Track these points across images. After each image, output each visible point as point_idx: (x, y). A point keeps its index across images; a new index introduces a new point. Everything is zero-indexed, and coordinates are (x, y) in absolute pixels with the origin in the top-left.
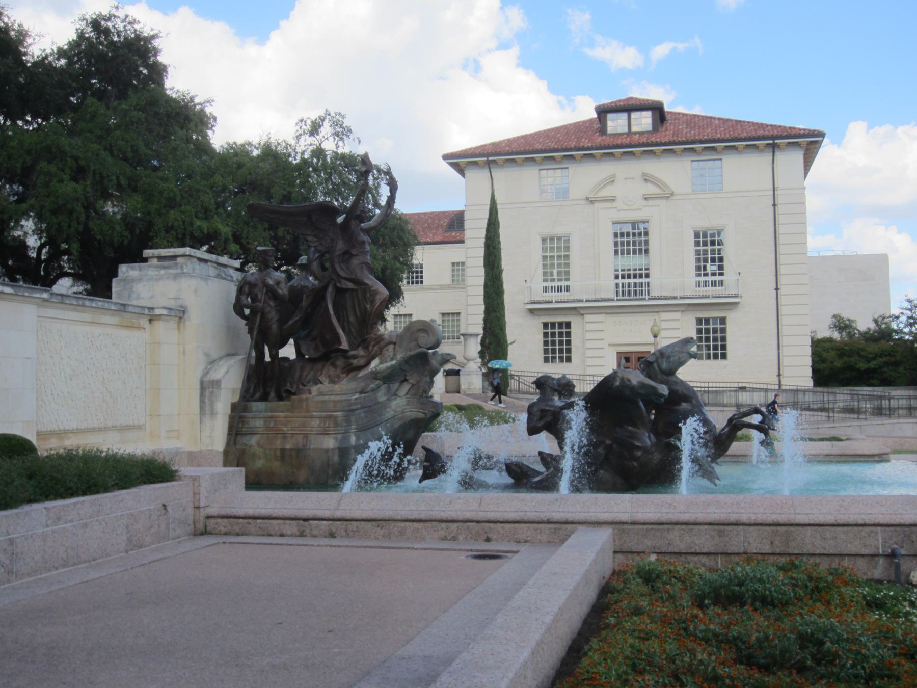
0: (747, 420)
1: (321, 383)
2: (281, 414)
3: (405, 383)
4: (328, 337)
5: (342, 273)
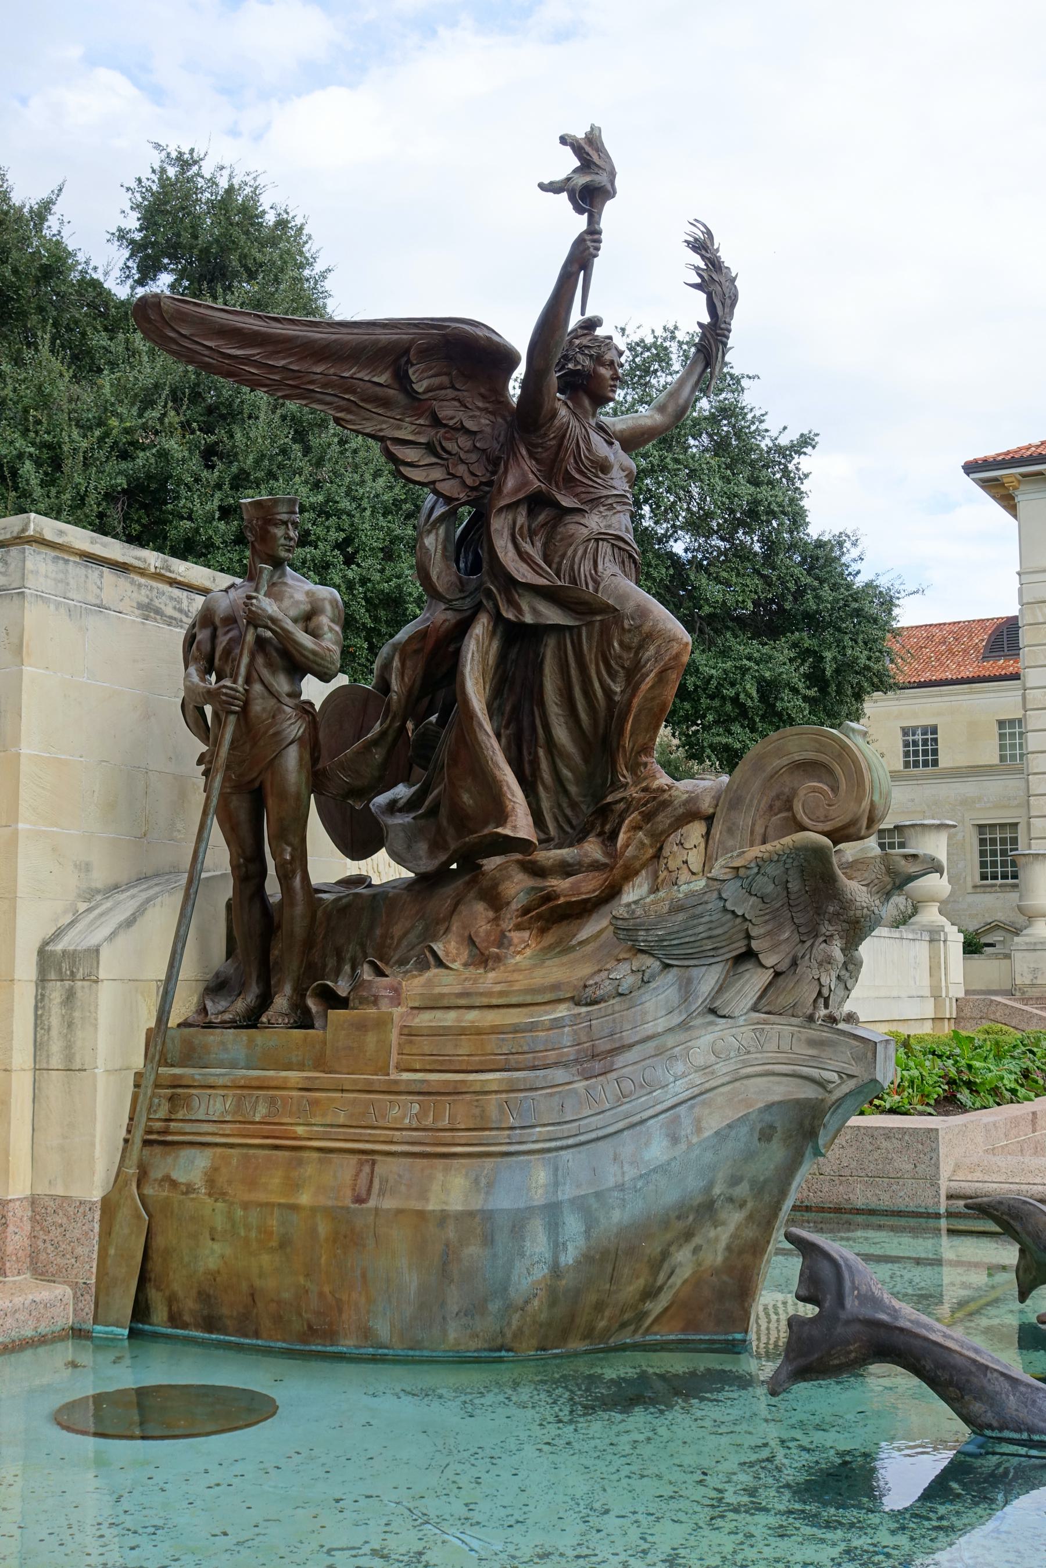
1: (440, 963)
2: (294, 1076)
3: (749, 965)
4: (466, 799)
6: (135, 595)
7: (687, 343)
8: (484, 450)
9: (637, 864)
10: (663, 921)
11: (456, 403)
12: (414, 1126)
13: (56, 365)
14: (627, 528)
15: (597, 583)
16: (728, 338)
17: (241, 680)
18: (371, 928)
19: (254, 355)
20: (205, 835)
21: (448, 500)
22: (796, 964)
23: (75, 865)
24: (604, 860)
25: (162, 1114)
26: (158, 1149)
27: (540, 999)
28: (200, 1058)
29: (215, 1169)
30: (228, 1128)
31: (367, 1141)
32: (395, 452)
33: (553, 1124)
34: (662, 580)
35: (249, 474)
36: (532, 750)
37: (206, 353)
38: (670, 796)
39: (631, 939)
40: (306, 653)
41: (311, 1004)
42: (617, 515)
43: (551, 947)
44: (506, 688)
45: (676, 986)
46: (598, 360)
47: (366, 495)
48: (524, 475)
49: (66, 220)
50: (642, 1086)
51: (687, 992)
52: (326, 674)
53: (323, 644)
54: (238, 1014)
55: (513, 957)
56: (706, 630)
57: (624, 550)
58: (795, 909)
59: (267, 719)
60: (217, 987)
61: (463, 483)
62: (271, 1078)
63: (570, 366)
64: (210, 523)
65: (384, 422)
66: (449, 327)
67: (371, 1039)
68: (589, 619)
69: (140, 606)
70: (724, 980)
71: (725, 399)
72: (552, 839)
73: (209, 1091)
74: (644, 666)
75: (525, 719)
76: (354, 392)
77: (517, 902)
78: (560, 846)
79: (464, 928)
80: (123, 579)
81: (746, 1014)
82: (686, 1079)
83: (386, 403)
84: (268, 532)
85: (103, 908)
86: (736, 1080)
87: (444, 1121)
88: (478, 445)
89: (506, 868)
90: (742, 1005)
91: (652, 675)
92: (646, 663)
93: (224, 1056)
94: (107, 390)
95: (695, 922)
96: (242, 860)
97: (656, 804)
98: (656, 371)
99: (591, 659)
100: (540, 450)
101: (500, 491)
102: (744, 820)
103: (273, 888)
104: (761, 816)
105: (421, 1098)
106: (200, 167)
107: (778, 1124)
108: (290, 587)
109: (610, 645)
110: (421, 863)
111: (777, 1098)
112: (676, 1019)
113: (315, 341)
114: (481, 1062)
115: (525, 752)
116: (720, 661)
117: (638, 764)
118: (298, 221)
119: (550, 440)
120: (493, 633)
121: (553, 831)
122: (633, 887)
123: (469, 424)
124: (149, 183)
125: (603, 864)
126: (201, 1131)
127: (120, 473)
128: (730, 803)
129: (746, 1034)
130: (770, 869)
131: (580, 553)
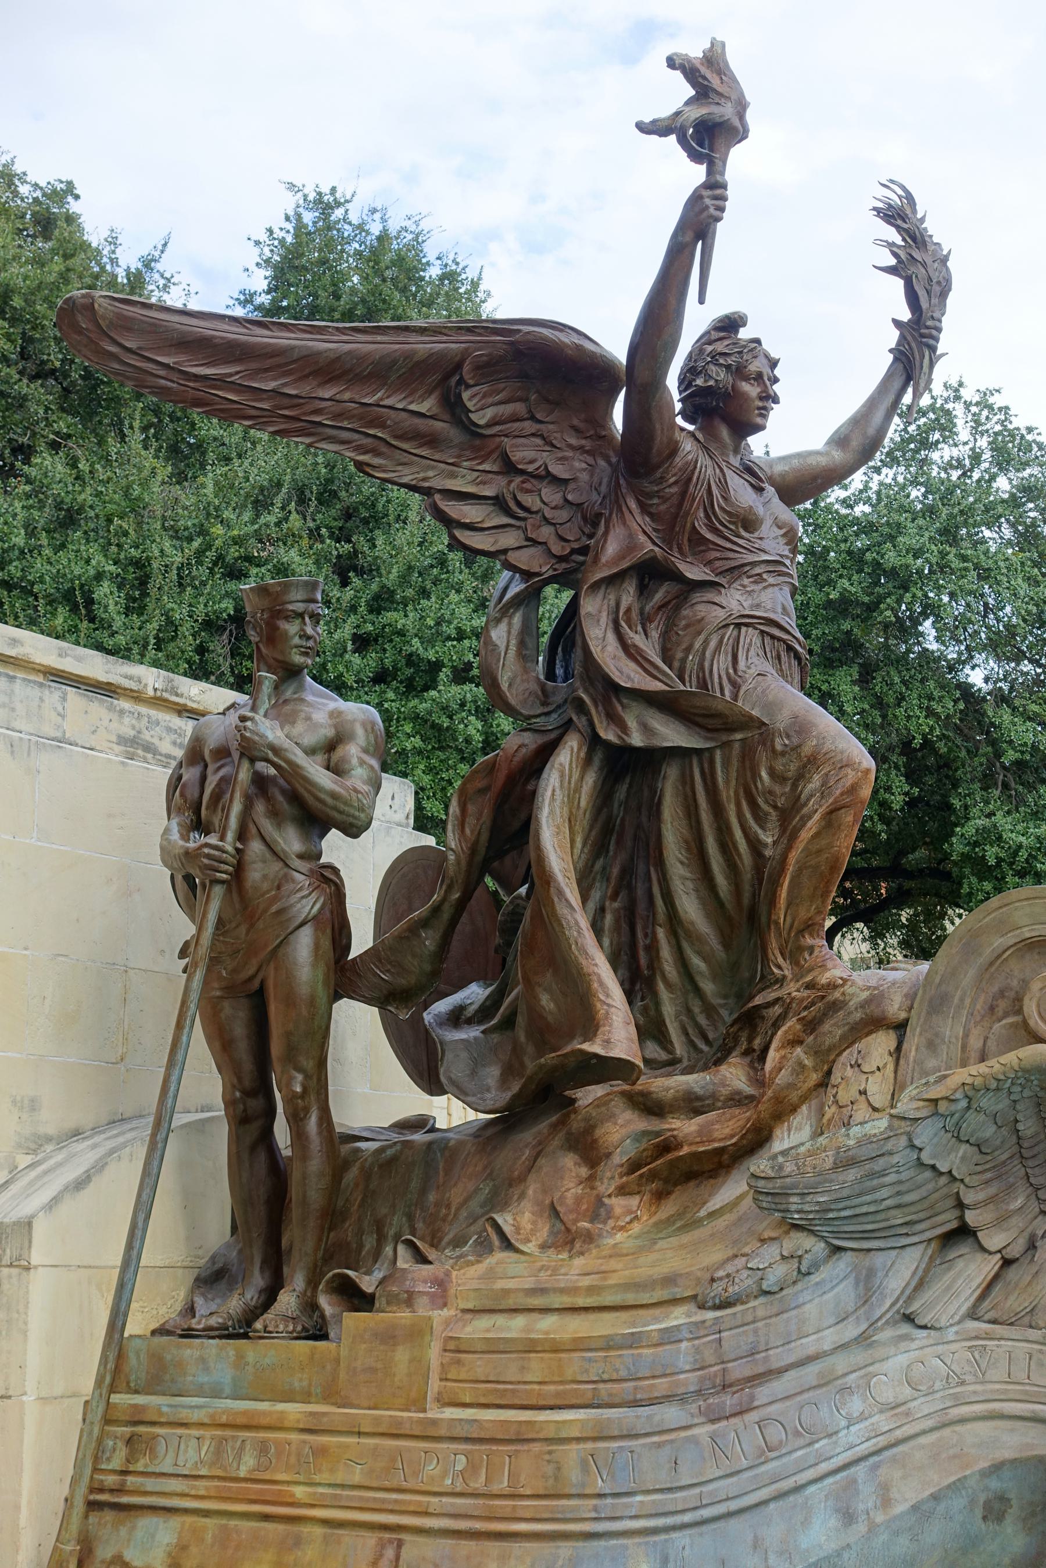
0: (910, 390)
1: (507, 1245)
2: (293, 1410)
3: (964, 1248)
4: (546, 1001)
5: (627, 674)
6: (115, 725)
7: (977, 404)
8: (579, 505)
9: (794, 1096)
10: (826, 1181)
11: (539, 441)
12: (458, 1490)
13: (148, 460)
14: (784, 608)
15: (736, 686)
16: (937, 340)
17: (230, 836)
18: (423, 1191)
19: (231, 375)
20: (180, 1057)
21: (527, 575)
22: (1035, 1247)
23: (14, 1102)
24: (748, 1090)
25: (116, 1463)
26: (109, 1516)
27: (645, 1298)
28: (173, 1381)
29: (183, 1548)
30: (201, 1487)
31: (392, 1511)
32: (446, 509)
33: (661, 1491)
34: (948, 717)
35: (393, 593)
36: (649, 931)
37: (162, 373)
38: (843, 994)
39: (781, 1210)
40: (323, 796)
41: (326, 1303)
42: (770, 590)
43: (669, 1221)
44: (613, 842)
45: (851, 1280)
46: (739, 372)
47: (547, 615)
48: (631, 536)
49: (193, 291)
50: (797, 1434)
51: (868, 1289)
52: (352, 825)
53: (348, 783)
54: (230, 1317)
55: (612, 1235)
56: (1013, 785)
57: (779, 639)
58: (1030, 1163)
59: (268, 891)
60: (214, 1278)
61: (549, 551)
62: (264, 1413)
63: (699, 382)
64: (341, 656)
65: (433, 468)
66: (519, 331)
67: (402, 1356)
68: (725, 737)
69: (122, 740)
70: (926, 1271)
71: (1031, 476)
72: (679, 1061)
73: (180, 1431)
74: (805, 804)
75: (639, 885)
76: (382, 426)
77: (622, 1153)
78: (689, 1071)
79: (545, 1192)
80: (96, 704)
81: (959, 1322)
82: (867, 1423)
83: (432, 441)
84: (278, 628)
85: (51, 1162)
86: (944, 1425)
87: (502, 1482)
88: (570, 497)
89: (606, 1103)
90: (952, 1309)
91: (817, 817)
92: (808, 800)
93: (203, 1379)
94: (210, 490)
95: (875, 1182)
96: (238, 1094)
97: (826, 1002)
98: (938, 442)
99: (728, 797)
100: (655, 501)
101: (596, 560)
102: (951, 1029)
103: (282, 1132)
104: (976, 1024)
105: (469, 1447)
106: (347, 211)
107: (1012, 1495)
108: (310, 705)
109: (756, 775)
110: (488, 1095)
111: (1008, 1454)
112: (851, 1331)
113: (319, 353)
114: (558, 1394)
115: (640, 934)
116: (1031, 824)
117: (800, 949)
118: (471, 274)
119: (670, 486)
120: (588, 761)
121: (679, 1048)
122: (789, 1130)
123: (556, 469)
124: (282, 234)
125: (747, 1097)
126: (167, 1490)
127: (227, 594)
128: (931, 1001)
129: (959, 1355)
130: (986, 1102)
131: (713, 644)
